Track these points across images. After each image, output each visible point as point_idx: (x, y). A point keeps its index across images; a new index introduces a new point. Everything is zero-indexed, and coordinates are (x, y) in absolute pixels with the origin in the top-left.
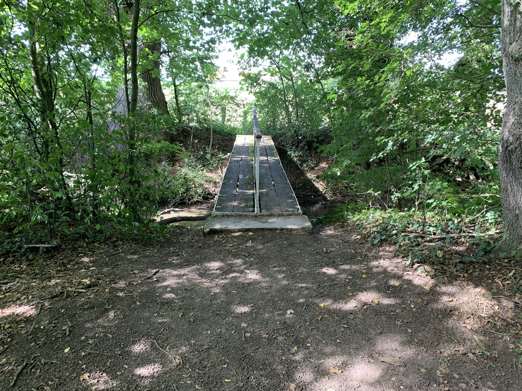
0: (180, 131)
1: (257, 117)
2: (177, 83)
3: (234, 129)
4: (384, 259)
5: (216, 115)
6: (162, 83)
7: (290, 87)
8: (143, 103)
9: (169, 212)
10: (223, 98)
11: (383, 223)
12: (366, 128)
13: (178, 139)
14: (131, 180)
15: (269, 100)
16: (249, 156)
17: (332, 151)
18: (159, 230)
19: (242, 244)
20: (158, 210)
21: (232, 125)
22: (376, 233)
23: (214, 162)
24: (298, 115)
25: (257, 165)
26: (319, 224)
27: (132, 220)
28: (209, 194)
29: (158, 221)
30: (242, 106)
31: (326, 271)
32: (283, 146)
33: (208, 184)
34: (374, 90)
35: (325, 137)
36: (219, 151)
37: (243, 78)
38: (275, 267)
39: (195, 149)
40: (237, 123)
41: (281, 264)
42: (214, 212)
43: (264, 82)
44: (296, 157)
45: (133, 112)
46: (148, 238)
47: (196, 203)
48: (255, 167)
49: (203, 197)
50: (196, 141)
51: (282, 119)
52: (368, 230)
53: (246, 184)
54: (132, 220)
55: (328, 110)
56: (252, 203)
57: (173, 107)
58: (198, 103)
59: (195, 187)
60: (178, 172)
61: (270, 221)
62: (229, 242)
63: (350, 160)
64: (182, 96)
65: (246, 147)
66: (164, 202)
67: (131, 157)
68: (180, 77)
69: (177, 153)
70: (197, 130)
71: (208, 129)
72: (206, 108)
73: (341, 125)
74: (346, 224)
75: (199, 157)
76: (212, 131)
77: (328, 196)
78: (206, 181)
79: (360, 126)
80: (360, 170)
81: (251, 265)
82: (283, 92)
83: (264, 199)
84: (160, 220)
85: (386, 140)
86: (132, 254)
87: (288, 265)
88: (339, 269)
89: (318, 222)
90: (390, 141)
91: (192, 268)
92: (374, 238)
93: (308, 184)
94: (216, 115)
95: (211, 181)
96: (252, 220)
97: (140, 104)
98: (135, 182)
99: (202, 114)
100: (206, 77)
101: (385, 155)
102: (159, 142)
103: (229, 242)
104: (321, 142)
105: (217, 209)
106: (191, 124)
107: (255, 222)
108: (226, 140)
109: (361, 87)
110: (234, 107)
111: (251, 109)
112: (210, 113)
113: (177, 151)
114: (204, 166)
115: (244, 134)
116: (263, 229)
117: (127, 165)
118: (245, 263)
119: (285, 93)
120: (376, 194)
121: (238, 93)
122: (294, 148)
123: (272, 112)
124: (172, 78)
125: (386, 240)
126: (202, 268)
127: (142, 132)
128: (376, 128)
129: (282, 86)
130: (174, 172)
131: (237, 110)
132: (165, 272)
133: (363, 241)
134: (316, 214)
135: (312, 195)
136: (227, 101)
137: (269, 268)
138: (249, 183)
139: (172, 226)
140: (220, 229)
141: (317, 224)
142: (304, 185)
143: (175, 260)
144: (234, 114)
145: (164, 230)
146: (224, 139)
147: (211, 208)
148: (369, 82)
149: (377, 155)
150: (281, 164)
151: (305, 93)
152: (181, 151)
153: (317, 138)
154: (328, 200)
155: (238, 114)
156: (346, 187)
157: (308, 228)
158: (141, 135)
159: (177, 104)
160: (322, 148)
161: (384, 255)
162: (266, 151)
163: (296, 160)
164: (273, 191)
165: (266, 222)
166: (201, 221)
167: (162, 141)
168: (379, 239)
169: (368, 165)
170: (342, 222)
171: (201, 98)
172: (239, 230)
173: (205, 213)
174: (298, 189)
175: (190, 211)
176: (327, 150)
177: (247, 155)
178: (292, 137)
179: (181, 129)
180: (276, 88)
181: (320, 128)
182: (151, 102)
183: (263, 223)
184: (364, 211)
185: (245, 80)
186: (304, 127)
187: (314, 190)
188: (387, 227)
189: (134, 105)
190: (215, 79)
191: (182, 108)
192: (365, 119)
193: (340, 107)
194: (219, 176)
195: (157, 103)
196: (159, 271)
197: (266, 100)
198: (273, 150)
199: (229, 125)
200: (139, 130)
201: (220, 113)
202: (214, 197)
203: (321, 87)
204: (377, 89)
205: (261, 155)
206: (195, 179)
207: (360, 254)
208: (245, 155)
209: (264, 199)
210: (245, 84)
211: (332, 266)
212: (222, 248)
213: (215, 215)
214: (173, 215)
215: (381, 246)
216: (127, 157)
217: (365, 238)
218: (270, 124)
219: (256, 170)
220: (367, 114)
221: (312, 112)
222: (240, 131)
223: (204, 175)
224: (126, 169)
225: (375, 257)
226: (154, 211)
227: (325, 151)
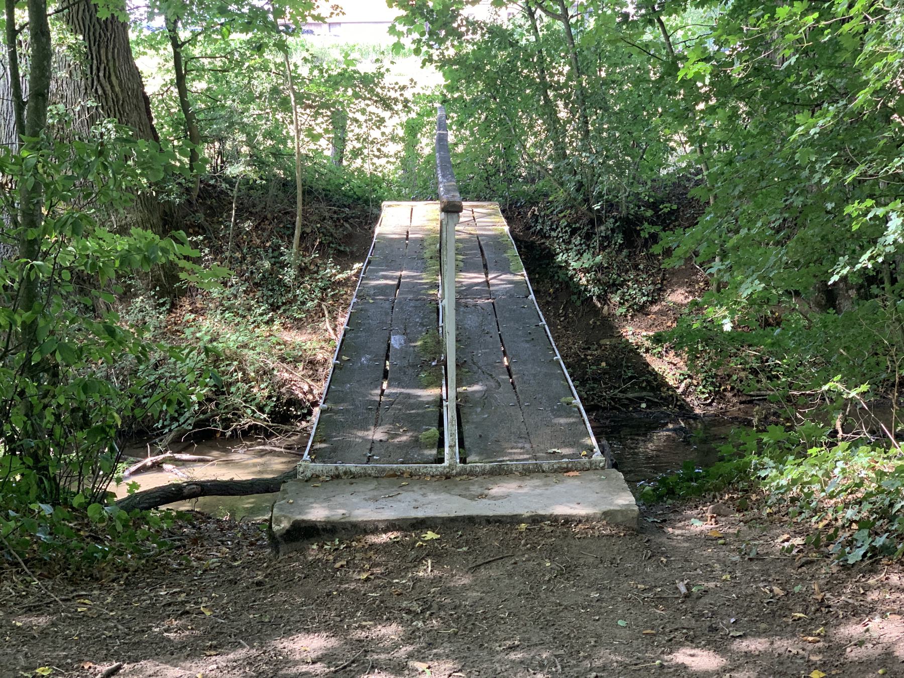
0: (194, 195)
1: (451, 139)
2: (184, 35)
3: (375, 181)
4: (883, 615)
5: (315, 138)
6: (132, 36)
7: (560, 42)
8: (70, 103)
9: (157, 467)
10: (335, 82)
11: (880, 491)
12: (813, 171)
13: (188, 220)
14: (29, 359)
15: (491, 84)
16: (424, 270)
17: (702, 249)
18: (120, 528)
19: (400, 571)
20: (118, 460)
21: (368, 168)
22: (854, 526)
23: (308, 294)
24: (588, 132)
25: (448, 304)
26: (664, 495)
27: (32, 495)
28: (294, 402)
29: (119, 498)
30: (400, 106)
31: (687, 661)
32: (542, 234)
33: (290, 367)
34: (835, 45)
35: (675, 206)
36: (324, 255)
37: (403, 13)
38: (512, 648)
39: (241, 255)
40: (383, 161)
41: (535, 640)
42: (307, 465)
43: (474, 26)
44: (586, 271)
45: (35, 134)
46: (83, 558)
47: (250, 434)
48: (444, 308)
49: (271, 414)
50: (248, 225)
51: (535, 145)
52: (830, 516)
53: (414, 366)
54: (32, 495)
55: (684, 116)
56: (434, 430)
57: (170, 114)
58: (252, 100)
59: (246, 380)
60: (188, 332)
61: (496, 490)
62: (356, 566)
63: (762, 279)
64: (200, 78)
65: (415, 240)
66: (141, 433)
67: (29, 284)
68: (192, 13)
69: (182, 269)
70: (251, 188)
71: (286, 185)
72: (279, 116)
73: (730, 163)
74: (754, 497)
75: (258, 277)
76: (299, 191)
77: (697, 403)
78: (283, 359)
79: (792, 166)
80: (799, 314)
81: (430, 645)
82: (538, 57)
83: (475, 418)
84: (126, 495)
85: (880, 212)
86: (29, 610)
87: (559, 640)
88: (733, 652)
89: (663, 490)
90: (893, 216)
91: (231, 656)
92: (850, 543)
93: (629, 366)
94: (315, 138)
95: (297, 360)
96: (435, 491)
97: (61, 106)
98: (43, 366)
99: (269, 135)
100: (279, 13)
101: (880, 260)
102: (123, 231)
103: (356, 566)
104: (668, 221)
105: (317, 456)
106: (232, 171)
107: (443, 496)
108: (346, 219)
109: (790, 36)
110: (372, 109)
111: (429, 114)
112: (293, 133)
113: (182, 263)
114: (274, 308)
115: (406, 198)
116: (471, 521)
117: (15, 311)
118: (409, 638)
119: (542, 60)
120: (853, 393)
121: (386, 64)
122: (577, 240)
123: (501, 123)
124: (167, 19)
125: (887, 550)
126: (266, 657)
127: (64, 199)
128: (845, 172)
129: (533, 39)
130: (172, 332)
131: (382, 120)
132: (141, 671)
133: (813, 556)
134: (656, 463)
135: (642, 399)
136: (350, 92)
137: (492, 653)
138: (424, 365)
139: (167, 516)
140: (327, 523)
141: (660, 498)
142: (615, 366)
143: (174, 630)
144: (375, 134)
145: (137, 526)
146: (340, 217)
147: (296, 451)
148: (817, 21)
149: (853, 262)
150: (532, 296)
151: (608, 58)
152: (198, 261)
153: (654, 206)
154: (696, 417)
155: (388, 131)
156: (754, 372)
157: (623, 512)
158: (62, 208)
159: (184, 105)
160: (668, 239)
161: (883, 601)
162: (480, 254)
163: (584, 281)
164: (505, 389)
165: (482, 496)
166: (268, 496)
167: (133, 230)
168: (866, 547)
169: (830, 297)
170: (741, 491)
171: (262, 83)
172: (391, 526)
173: (280, 467)
174: (595, 380)
175: (228, 463)
176: (683, 248)
177: (417, 270)
178: (570, 204)
179: (197, 187)
180: (512, 45)
181: (663, 172)
182: (98, 98)
183: (473, 498)
184: (813, 451)
185: (408, 20)
186: (609, 170)
187: (648, 382)
188: (891, 505)
189: (39, 112)
190: (310, 20)
191: (201, 116)
192: (811, 143)
193: (723, 105)
194: (321, 340)
195: (116, 102)
196: (119, 668)
197: (481, 86)
198: (504, 248)
199: (360, 170)
200: (55, 193)
201: (326, 131)
202: (310, 413)
203: (663, 39)
204: (846, 43)
205: (465, 266)
206: (245, 351)
207: (804, 600)
208: (412, 269)
209: (476, 415)
210: (409, 32)
211: (709, 643)
212: (332, 587)
213: (309, 474)
214: (171, 476)
215: (873, 571)
216: (16, 286)
217: (817, 544)
218: (495, 164)
219: (447, 320)
220: (811, 126)
221: (635, 117)
222: (395, 189)
223: (274, 340)
224: (12, 324)
225: (854, 608)
226: (107, 465)
227: (678, 252)
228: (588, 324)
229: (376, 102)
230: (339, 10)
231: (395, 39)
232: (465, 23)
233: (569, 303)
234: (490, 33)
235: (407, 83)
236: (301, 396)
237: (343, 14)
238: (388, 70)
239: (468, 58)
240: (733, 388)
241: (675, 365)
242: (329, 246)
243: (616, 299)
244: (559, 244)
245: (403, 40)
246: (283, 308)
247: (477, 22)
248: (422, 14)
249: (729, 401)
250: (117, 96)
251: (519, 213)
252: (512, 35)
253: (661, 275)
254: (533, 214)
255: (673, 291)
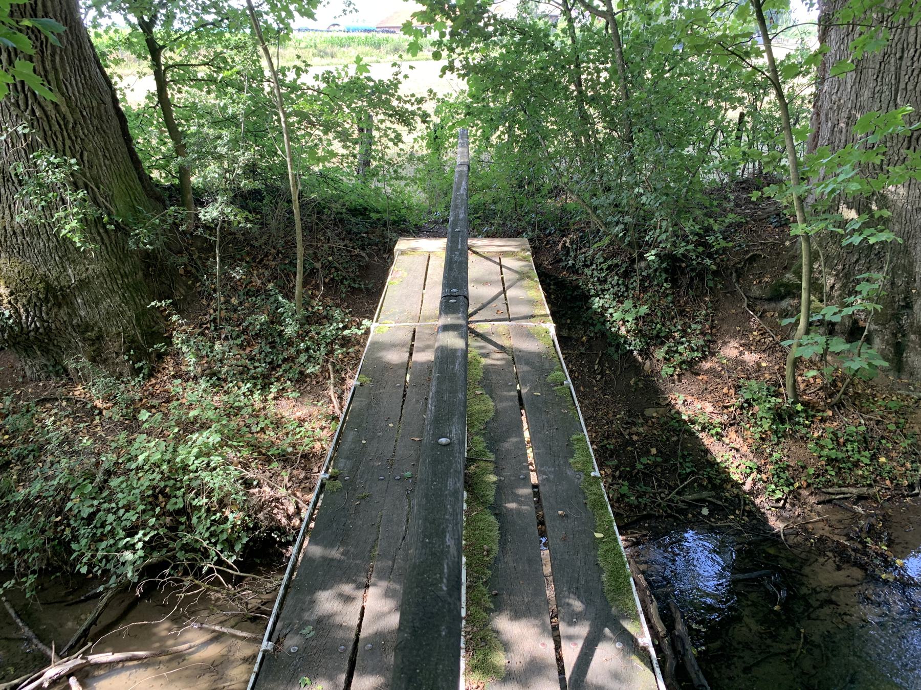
121: (405, 69)
228: (628, 385)
229: (391, 116)
230: (352, 6)
231: (411, 39)
232: (492, 21)
234: (521, 33)
235: (426, 95)
236: (284, 521)
237: (356, 11)
238: (406, 77)
239: (496, 65)
240: (809, 485)
241: (737, 450)
242: (342, 283)
243: (660, 353)
245: (421, 41)
247: (506, 20)
248: (442, 11)
249: (805, 503)
250: (64, 118)
251: (548, 242)
252: (547, 36)
253: (710, 322)
254: (564, 247)
255: (725, 343)
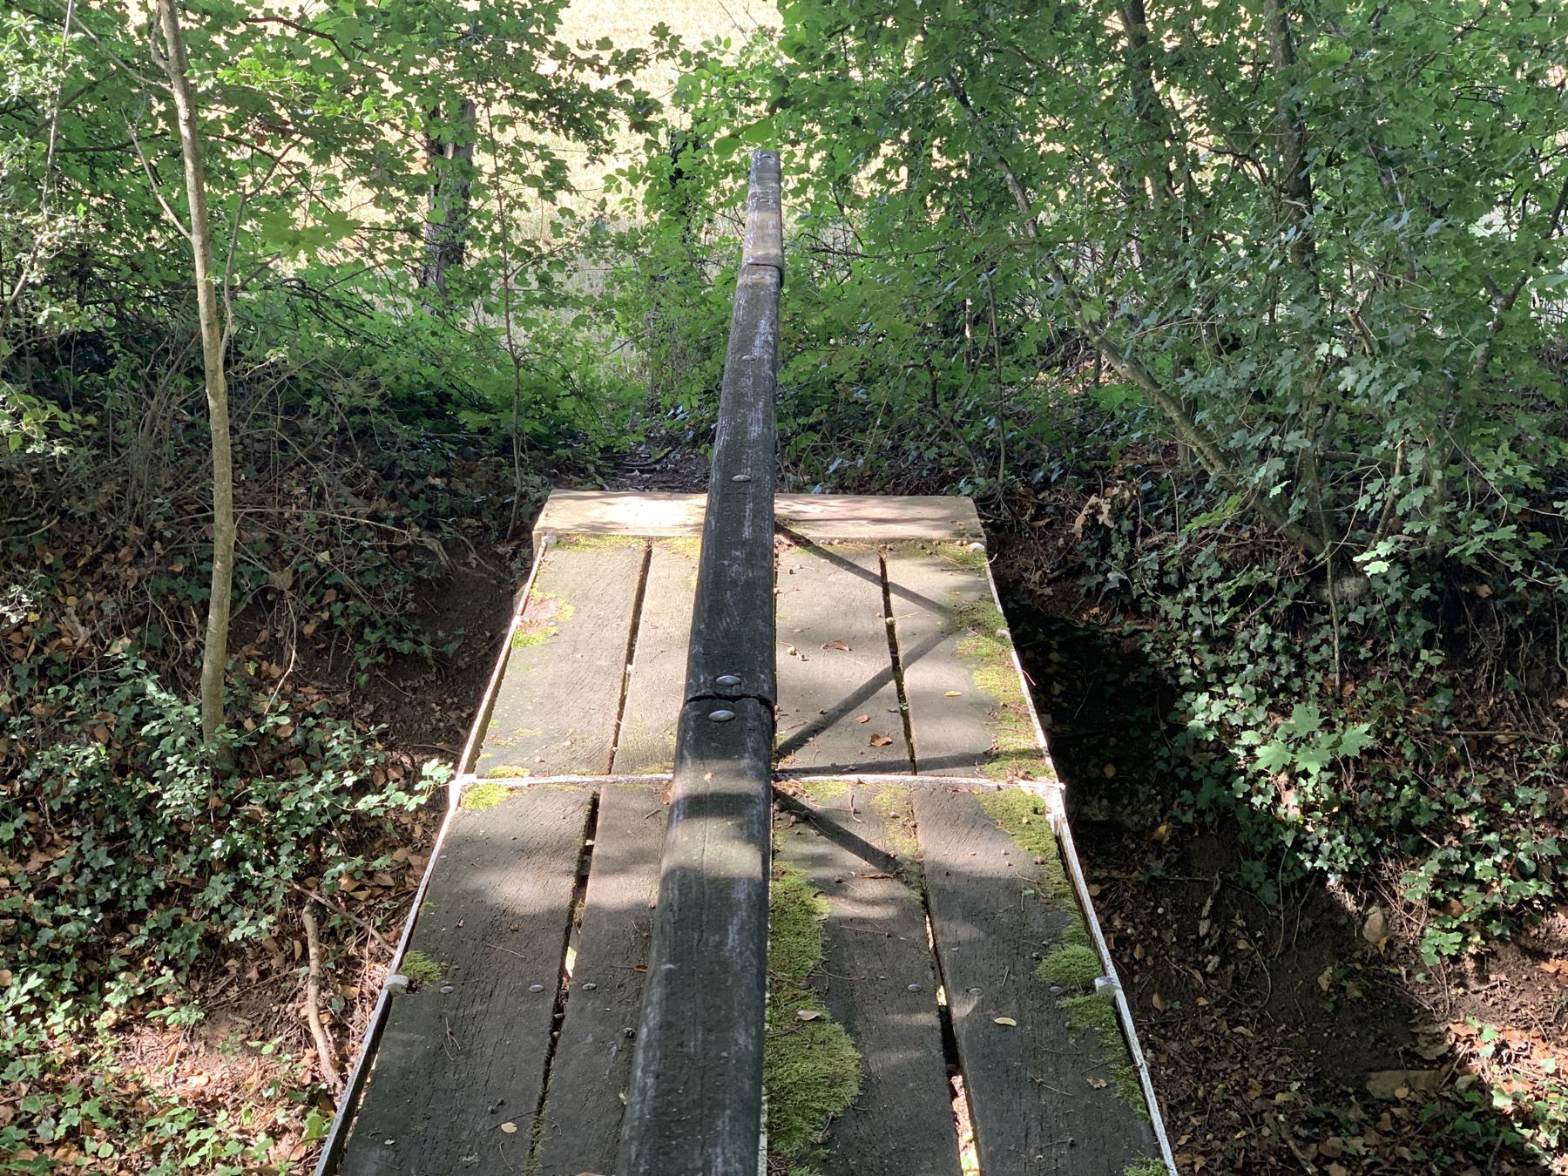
228: (1312, 989)
229: (533, 106)
233: (1235, 895)
235: (646, 41)
242: (359, 637)
243: (1415, 883)
244: (1188, 649)
246: (154, 919)
251: (1041, 508)
254: (1093, 525)
